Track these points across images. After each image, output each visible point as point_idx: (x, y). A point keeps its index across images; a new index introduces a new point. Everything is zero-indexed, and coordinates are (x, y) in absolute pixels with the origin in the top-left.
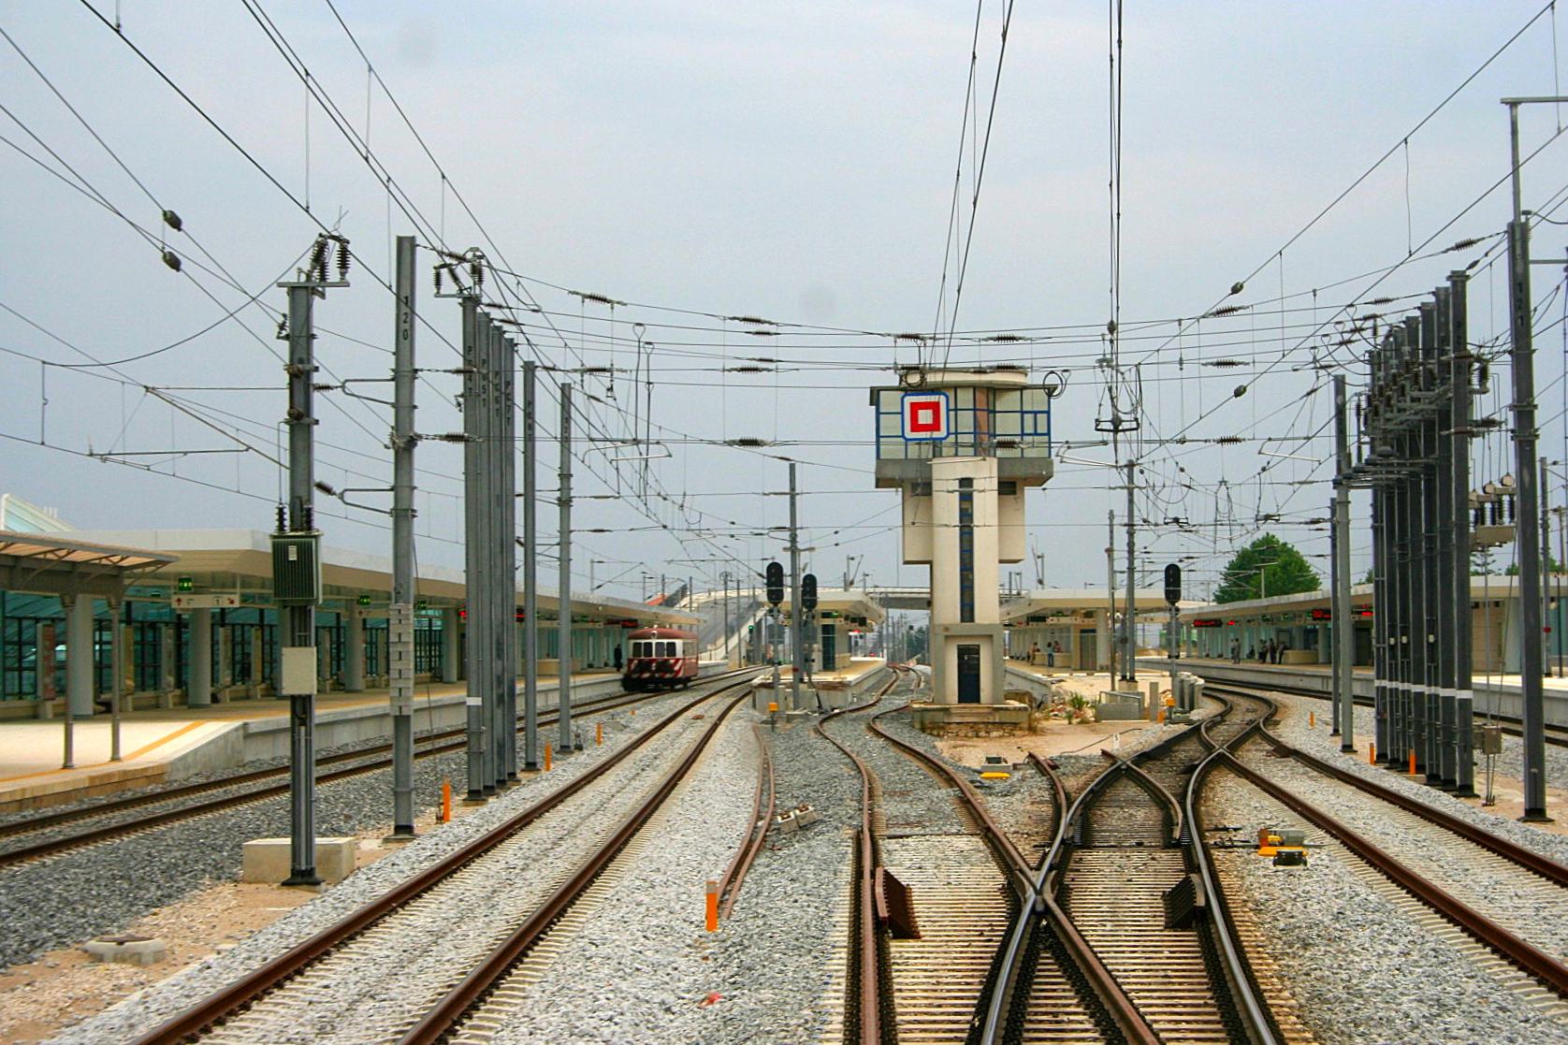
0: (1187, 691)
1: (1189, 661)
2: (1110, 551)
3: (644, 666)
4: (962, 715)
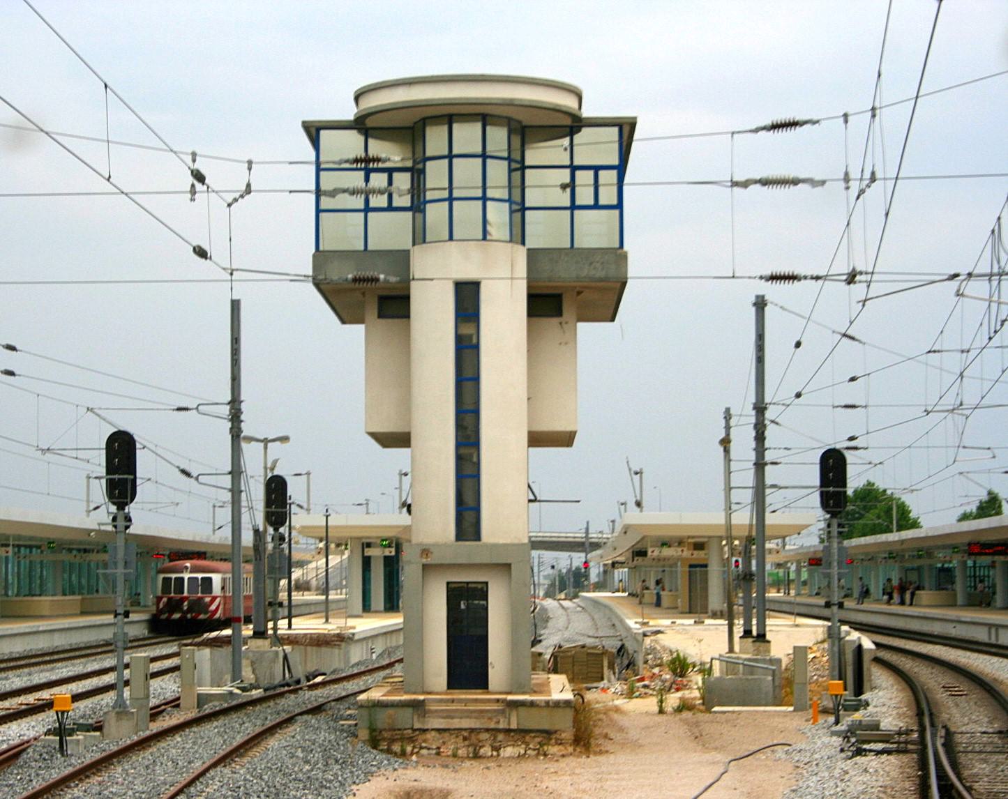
0: (849, 657)
1: (799, 600)
2: (725, 442)
3: (174, 605)
4: (449, 715)
